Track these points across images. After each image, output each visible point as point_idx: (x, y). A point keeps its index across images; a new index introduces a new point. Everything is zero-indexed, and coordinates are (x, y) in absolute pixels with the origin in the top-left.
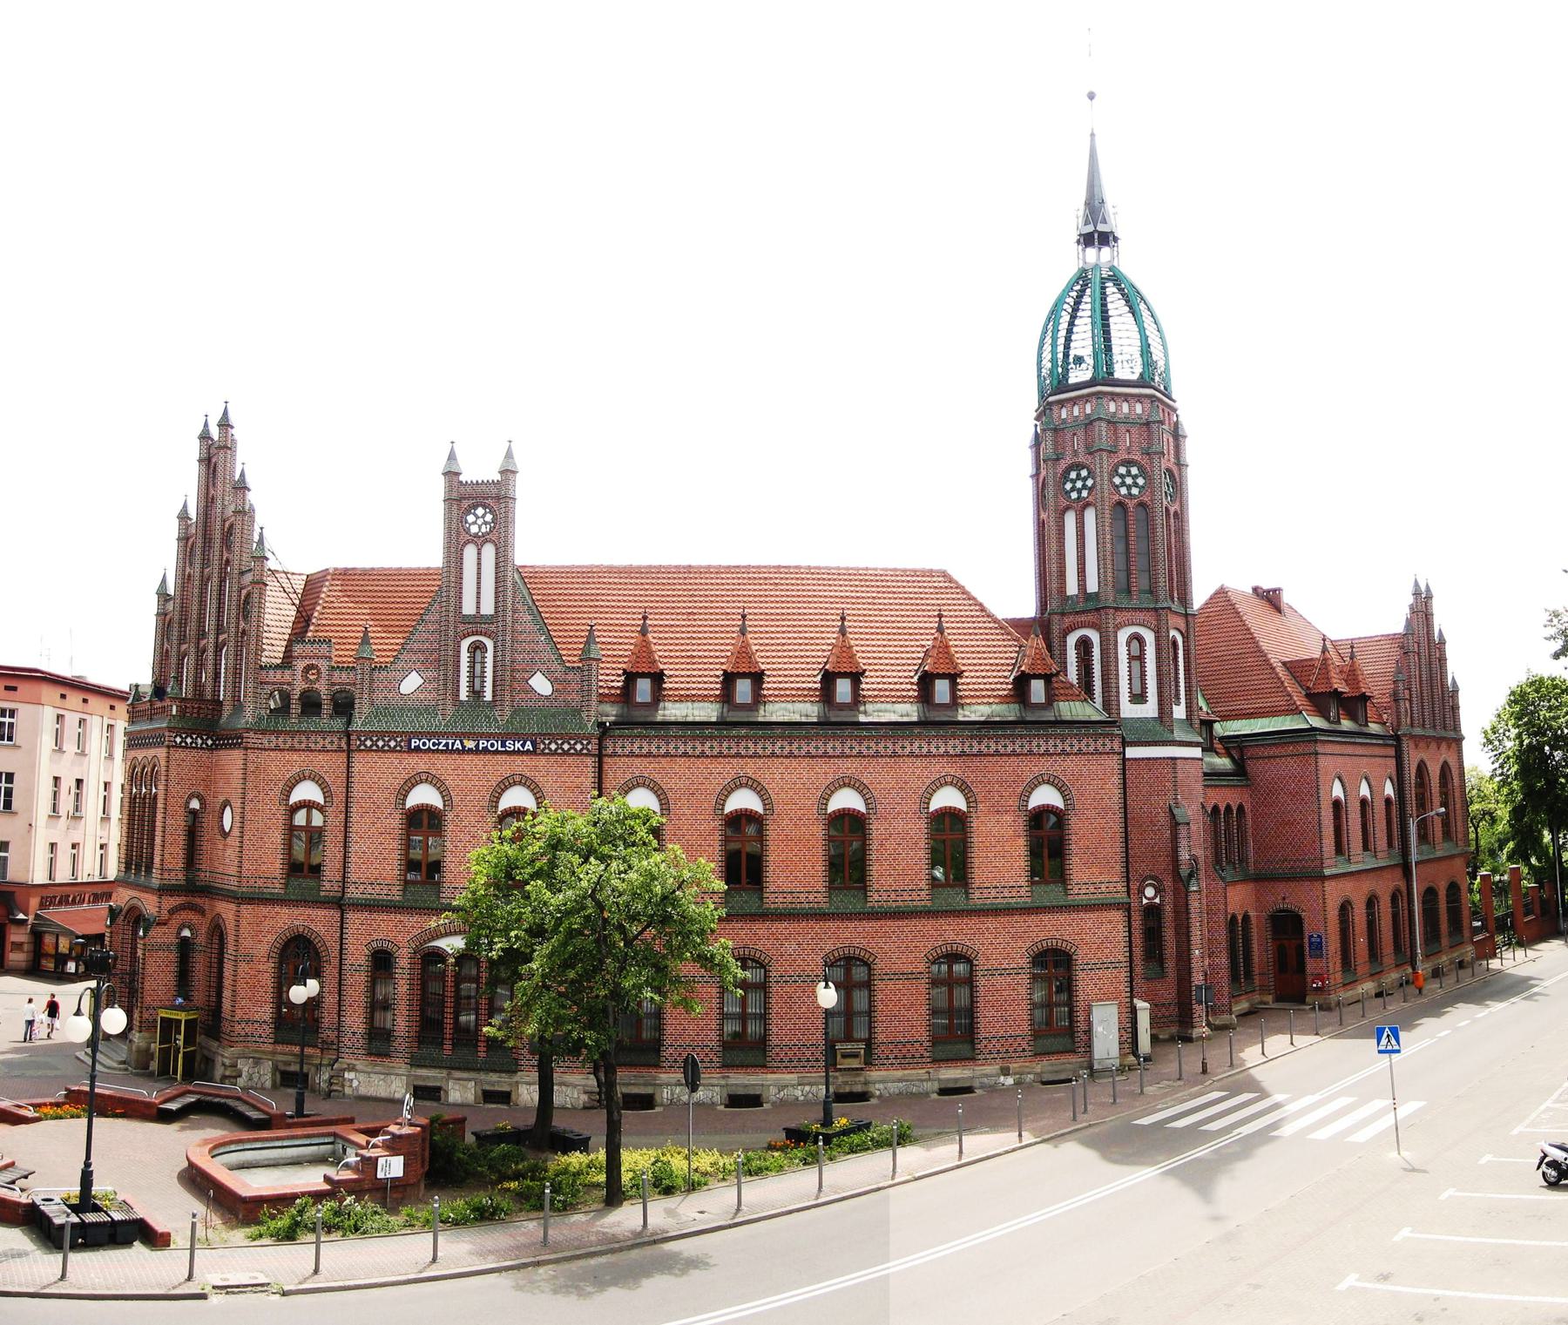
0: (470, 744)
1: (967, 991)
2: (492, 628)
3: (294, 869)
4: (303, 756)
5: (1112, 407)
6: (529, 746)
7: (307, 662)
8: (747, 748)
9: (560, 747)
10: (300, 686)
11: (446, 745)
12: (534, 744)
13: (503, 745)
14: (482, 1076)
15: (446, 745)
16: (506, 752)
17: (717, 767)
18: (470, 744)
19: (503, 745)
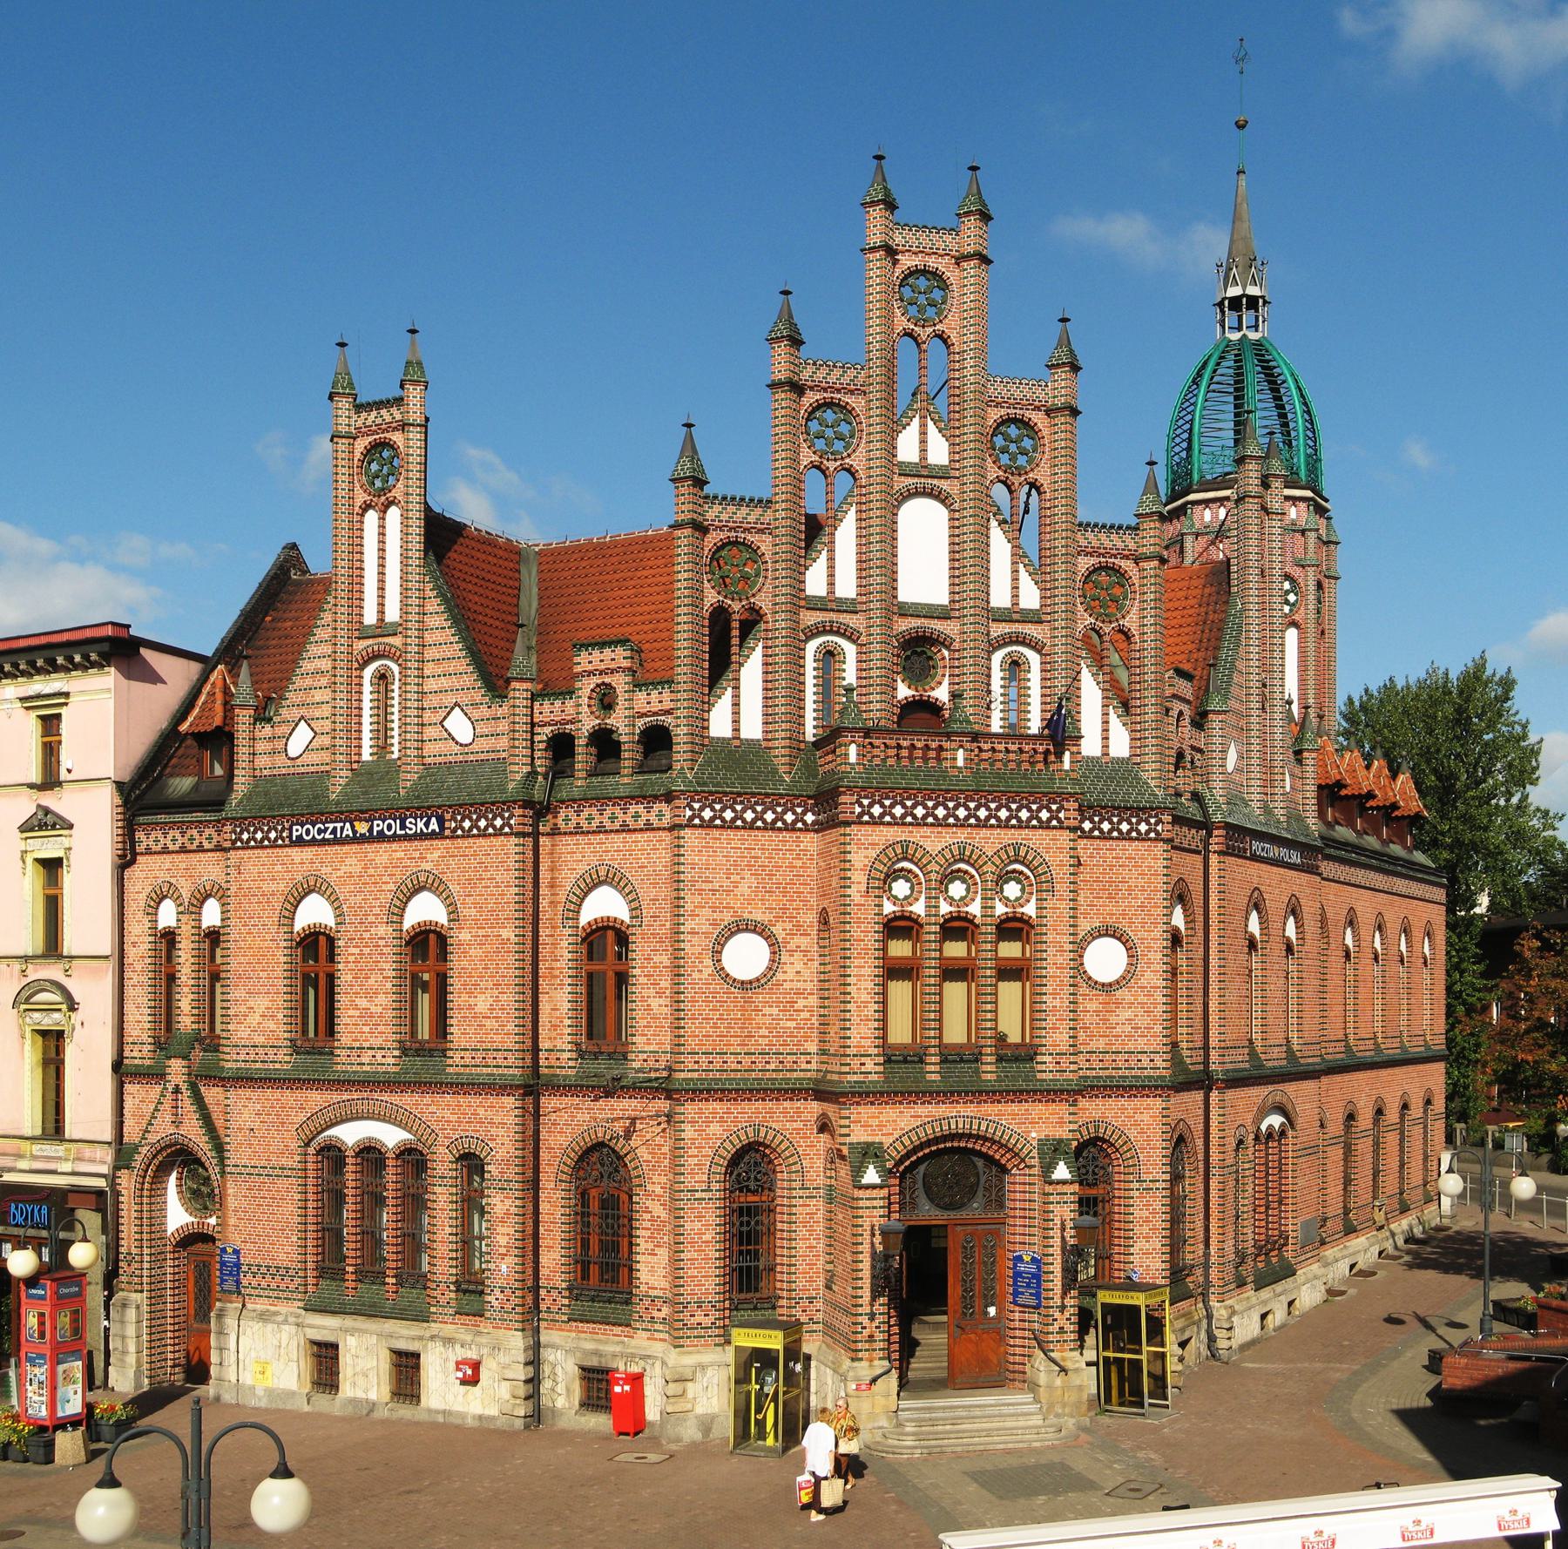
0: (362, 828)
1: (892, 1040)
2: (396, 641)
3: (410, 1048)
4: (618, 839)
5: (1208, 515)
6: (434, 826)
7: (597, 680)
8: (613, 818)
9: (779, 818)
10: (588, 723)
11: (334, 831)
12: (441, 822)
13: (403, 827)
14: (391, 1325)
15: (334, 831)
16: (407, 838)
17: (382, 854)
18: (362, 828)
19: (403, 827)
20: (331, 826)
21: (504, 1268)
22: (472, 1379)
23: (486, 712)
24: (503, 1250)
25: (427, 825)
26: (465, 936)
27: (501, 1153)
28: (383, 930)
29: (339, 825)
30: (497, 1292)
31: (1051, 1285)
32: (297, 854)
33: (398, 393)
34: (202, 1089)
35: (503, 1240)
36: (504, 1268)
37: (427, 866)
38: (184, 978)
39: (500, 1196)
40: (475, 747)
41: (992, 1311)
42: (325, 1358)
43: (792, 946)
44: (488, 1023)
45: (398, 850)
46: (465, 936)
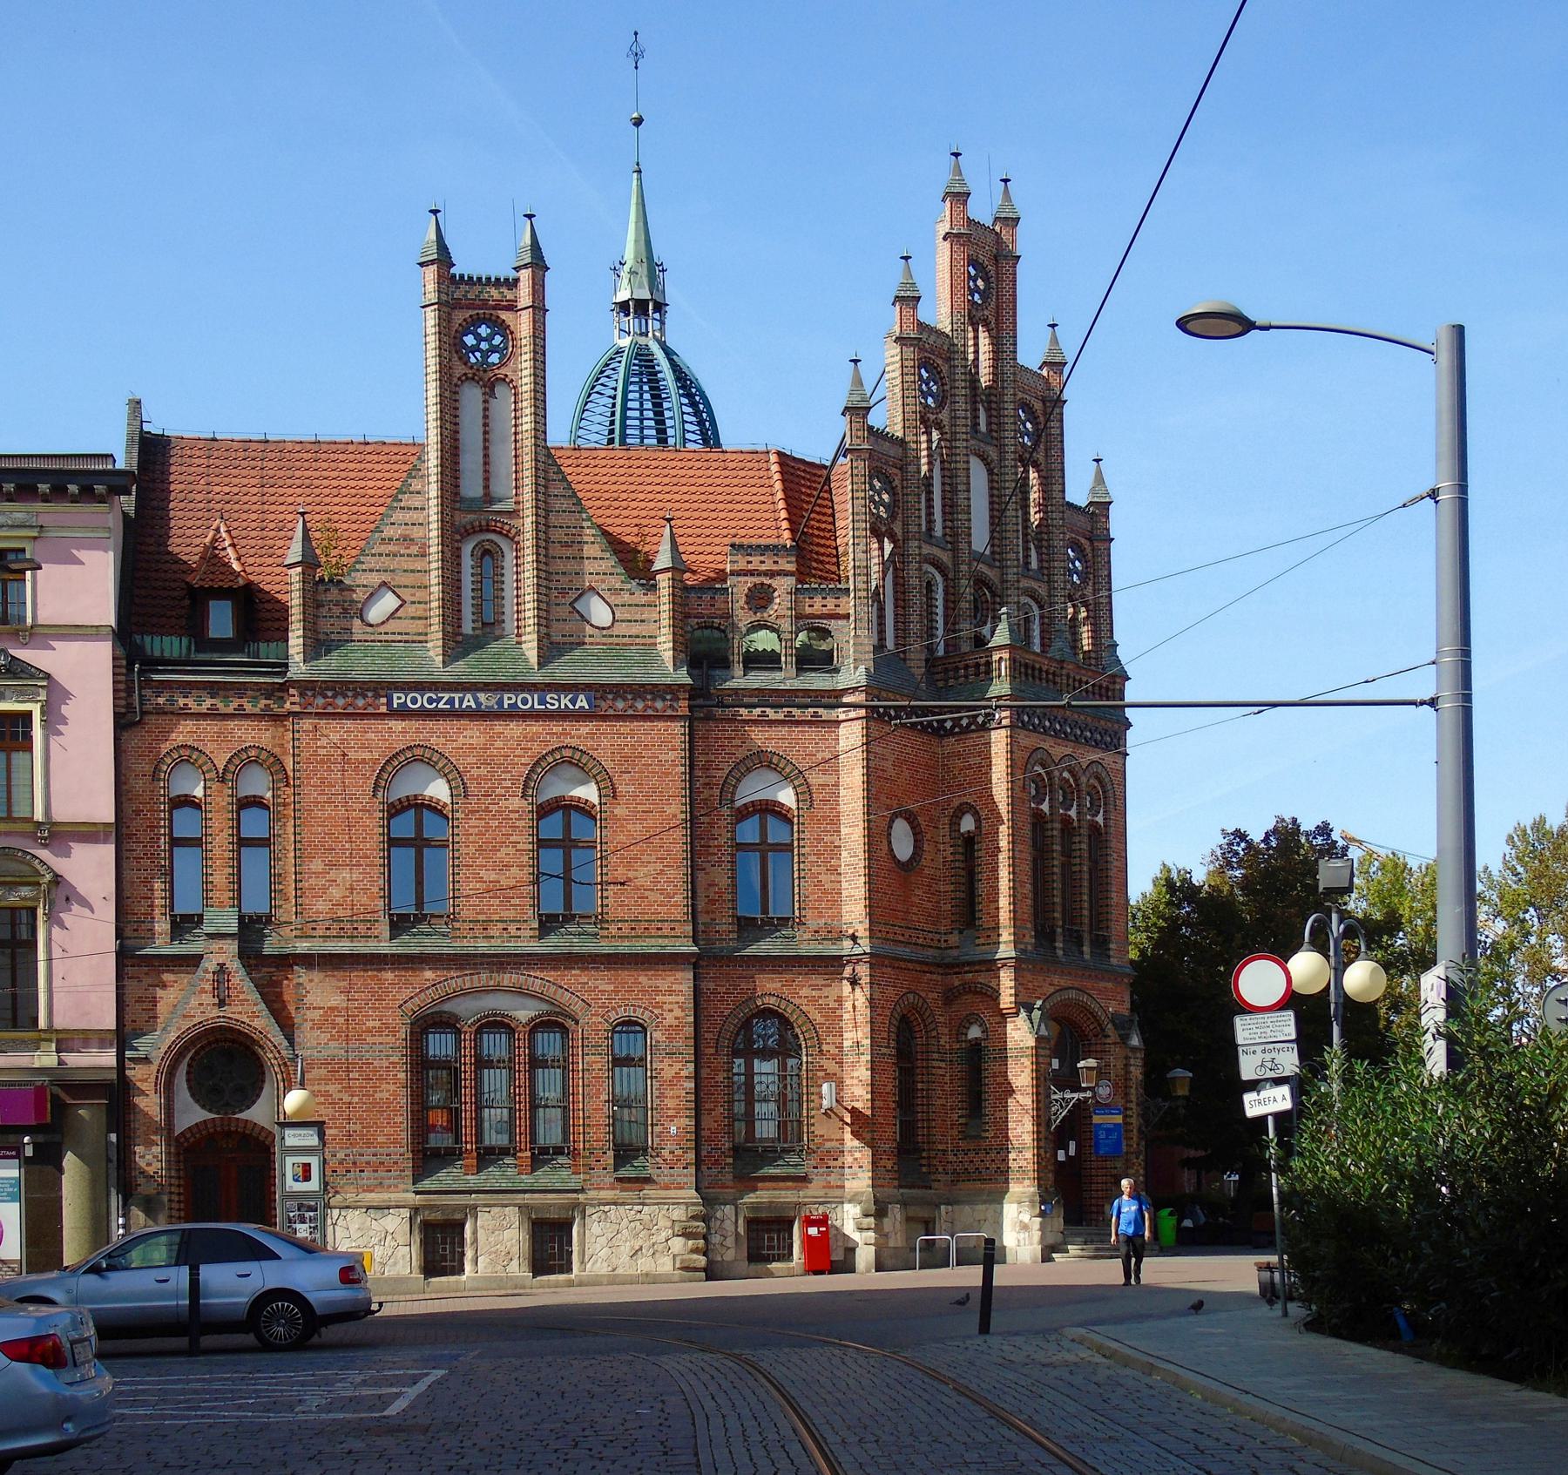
11: (451, 701)
15: (451, 701)
20: (446, 696)
21: (673, 1129)
22: (634, 1249)
23: (626, 597)
24: (671, 1113)
25: (573, 702)
26: (619, 811)
27: (670, 1019)
28: (516, 803)
29: (457, 696)
30: (665, 1153)
31: (842, 498)
32: (397, 725)
33: (512, 274)
34: (148, 951)
35: (670, 1103)
36: (673, 1129)
37: (574, 742)
38: (217, 851)
39: (667, 1061)
40: (615, 631)
41: (1055, 1064)
42: (550, 1244)
43: (929, 836)
44: (652, 896)
45: (536, 727)
46: (619, 811)
